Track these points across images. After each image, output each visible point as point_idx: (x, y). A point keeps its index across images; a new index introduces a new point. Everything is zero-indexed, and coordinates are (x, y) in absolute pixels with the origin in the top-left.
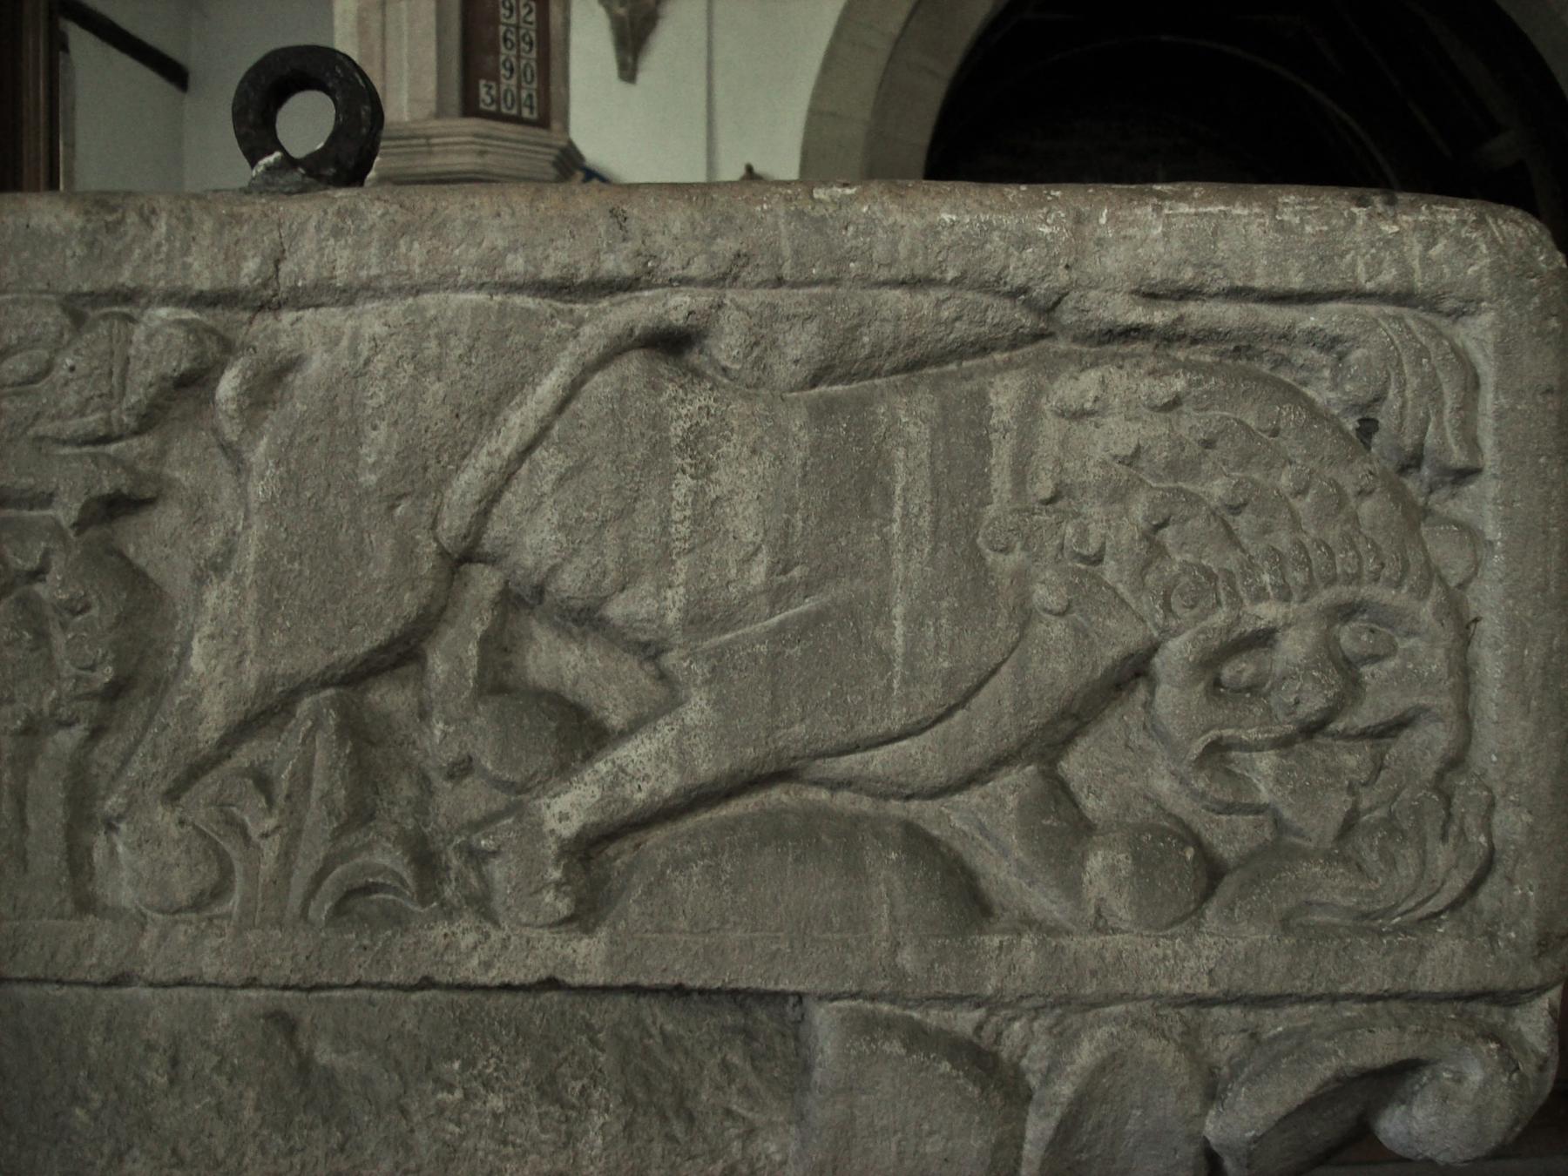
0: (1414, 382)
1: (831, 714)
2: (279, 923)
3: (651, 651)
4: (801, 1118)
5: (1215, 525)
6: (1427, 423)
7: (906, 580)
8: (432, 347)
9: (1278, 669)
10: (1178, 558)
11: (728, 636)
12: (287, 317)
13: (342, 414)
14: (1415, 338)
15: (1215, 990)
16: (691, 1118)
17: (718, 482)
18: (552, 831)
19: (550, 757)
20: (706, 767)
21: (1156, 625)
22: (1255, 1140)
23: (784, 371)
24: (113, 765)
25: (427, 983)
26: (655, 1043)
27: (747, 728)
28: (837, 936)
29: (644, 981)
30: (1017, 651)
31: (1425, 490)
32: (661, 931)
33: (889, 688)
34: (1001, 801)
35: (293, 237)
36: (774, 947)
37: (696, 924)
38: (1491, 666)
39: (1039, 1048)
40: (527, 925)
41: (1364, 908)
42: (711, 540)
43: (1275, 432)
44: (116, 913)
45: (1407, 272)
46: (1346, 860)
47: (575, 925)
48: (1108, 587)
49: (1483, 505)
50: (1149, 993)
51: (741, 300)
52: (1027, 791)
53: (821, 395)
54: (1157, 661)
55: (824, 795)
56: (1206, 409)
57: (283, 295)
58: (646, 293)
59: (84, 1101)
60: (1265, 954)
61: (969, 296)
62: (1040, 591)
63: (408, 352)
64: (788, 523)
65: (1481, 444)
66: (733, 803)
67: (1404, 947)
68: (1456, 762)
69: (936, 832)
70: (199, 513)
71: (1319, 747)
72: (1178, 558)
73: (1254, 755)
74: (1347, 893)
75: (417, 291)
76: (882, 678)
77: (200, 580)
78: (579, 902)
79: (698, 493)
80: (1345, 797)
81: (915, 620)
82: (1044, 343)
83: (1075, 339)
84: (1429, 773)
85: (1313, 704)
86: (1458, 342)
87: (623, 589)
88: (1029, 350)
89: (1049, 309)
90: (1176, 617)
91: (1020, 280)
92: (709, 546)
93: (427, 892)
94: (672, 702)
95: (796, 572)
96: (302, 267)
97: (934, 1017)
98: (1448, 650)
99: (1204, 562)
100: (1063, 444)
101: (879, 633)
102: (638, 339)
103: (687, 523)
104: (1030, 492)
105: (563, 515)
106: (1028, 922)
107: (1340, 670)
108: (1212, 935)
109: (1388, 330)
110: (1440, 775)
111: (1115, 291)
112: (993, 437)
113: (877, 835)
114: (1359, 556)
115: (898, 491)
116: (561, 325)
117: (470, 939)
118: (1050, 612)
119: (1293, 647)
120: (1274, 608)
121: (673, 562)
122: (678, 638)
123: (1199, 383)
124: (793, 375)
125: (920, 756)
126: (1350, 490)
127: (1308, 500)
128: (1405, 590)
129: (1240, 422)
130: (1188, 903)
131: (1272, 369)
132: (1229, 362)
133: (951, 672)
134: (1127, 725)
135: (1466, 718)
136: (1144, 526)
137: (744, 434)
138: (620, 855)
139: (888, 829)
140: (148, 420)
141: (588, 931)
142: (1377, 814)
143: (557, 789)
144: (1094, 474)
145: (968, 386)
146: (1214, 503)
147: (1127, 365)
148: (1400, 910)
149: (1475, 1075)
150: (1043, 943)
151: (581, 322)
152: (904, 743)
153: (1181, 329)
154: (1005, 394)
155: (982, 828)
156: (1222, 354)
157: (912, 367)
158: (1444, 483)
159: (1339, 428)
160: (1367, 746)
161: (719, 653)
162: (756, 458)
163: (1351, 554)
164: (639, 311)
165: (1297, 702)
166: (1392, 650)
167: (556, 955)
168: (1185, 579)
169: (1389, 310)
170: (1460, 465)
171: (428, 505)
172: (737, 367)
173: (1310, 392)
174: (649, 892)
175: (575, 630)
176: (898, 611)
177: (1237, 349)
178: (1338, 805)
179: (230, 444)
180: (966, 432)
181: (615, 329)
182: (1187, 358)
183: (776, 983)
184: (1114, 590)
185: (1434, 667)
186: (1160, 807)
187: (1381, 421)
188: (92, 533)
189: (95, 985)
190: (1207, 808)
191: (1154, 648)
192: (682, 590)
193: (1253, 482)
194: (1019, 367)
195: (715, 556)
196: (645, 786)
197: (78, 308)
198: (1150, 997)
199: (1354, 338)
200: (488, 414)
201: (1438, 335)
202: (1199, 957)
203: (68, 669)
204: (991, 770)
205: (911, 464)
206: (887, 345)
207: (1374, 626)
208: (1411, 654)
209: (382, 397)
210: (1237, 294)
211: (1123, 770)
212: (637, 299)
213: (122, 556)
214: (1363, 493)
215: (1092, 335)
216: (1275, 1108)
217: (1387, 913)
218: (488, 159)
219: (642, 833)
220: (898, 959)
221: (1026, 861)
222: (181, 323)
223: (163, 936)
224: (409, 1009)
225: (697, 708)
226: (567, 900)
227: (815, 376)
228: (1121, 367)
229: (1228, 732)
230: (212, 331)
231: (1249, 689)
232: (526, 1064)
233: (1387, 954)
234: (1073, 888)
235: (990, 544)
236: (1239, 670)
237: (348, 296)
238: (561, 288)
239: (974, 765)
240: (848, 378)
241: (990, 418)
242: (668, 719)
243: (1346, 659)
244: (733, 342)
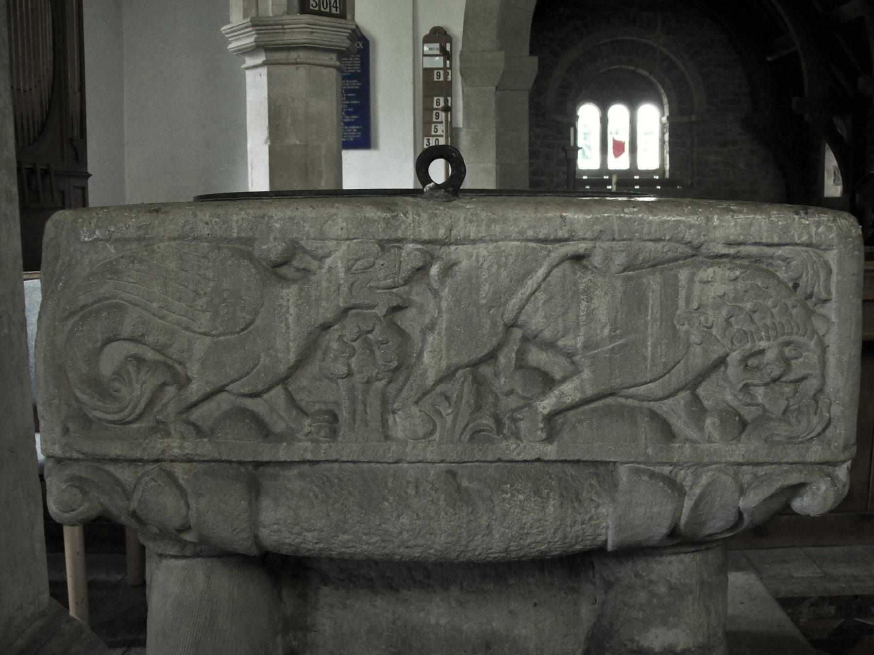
0: (811, 272)
2: (452, 442)
3: (570, 355)
4: (614, 501)
8: (503, 259)
9: (765, 361)
12: (453, 248)
13: (474, 281)
16: (580, 502)
20: (590, 392)
22: (755, 507)
23: (614, 268)
24: (394, 392)
25: (499, 460)
26: (569, 478)
29: (568, 459)
35: (455, 222)
38: (832, 361)
39: (689, 478)
43: (767, 288)
44: (397, 440)
45: (811, 237)
46: (785, 421)
49: (831, 310)
51: (602, 245)
55: (624, 400)
57: (452, 240)
59: (387, 500)
61: (673, 244)
62: (693, 337)
63: (495, 261)
68: (820, 390)
70: (422, 310)
74: (786, 431)
75: (497, 241)
77: (424, 333)
78: (548, 434)
79: (588, 307)
81: (655, 346)
83: (705, 257)
84: (811, 393)
85: (776, 373)
88: (689, 260)
89: (698, 248)
91: (689, 239)
93: (499, 431)
95: (618, 332)
96: (459, 231)
97: (657, 469)
100: (701, 291)
106: (687, 440)
110: (815, 395)
113: (641, 413)
116: (544, 253)
117: (514, 446)
119: (771, 355)
122: (580, 351)
126: (790, 306)
135: (823, 376)
138: (560, 419)
140: (406, 282)
141: (551, 443)
144: (711, 300)
145: (671, 273)
147: (722, 266)
149: (823, 488)
151: (550, 252)
154: (683, 275)
155: (672, 410)
157: (653, 266)
160: (792, 386)
161: (593, 357)
164: (570, 248)
168: (737, 334)
169: (804, 248)
171: (501, 310)
173: (778, 274)
174: (570, 431)
176: (649, 343)
178: (783, 403)
179: (435, 290)
186: (728, 404)
188: (387, 318)
189: (389, 463)
191: (727, 355)
197: (384, 245)
200: (521, 280)
201: (820, 256)
203: (381, 362)
209: (487, 276)
210: (756, 244)
211: (716, 392)
213: (396, 324)
214: (794, 307)
216: (762, 497)
217: (798, 437)
218: (315, 36)
222: (418, 250)
223: (414, 447)
224: (492, 469)
225: (586, 374)
230: (427, 252)
232: (530, 485)
234: (701, 429)
235: (678, 323)
237: (474, 242)
238: (545, 241)
239: (672, 391)
240: (634, 270)
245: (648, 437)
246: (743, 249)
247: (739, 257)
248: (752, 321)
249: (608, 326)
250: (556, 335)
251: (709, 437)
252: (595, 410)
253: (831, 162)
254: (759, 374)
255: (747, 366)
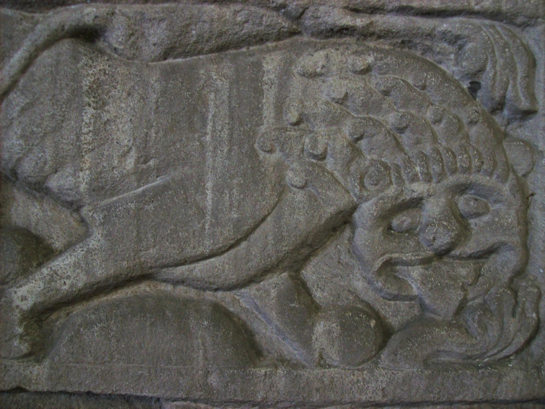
0: (501, 61)
1: (170, 243)
3: (75, 206)
5: (389, 139)
6: (508, 84)
7: (213, 168)
9: (424, 221)
10: (369, 157)
11: (115, 199)
14: (501, 37)
15: (385, 399)
17: (108, 112)
18: (18, 306)
19: (17, 265)
20: (101, 272)
21: (355, 195)
23: (149, 50)
27: (123, 251)
28: (174, 367)
29: (70, 390)
30: (276, 208)
31: (505, 122)
32: (78, 363)
33: (203, 228)
34: (267, 292)
36: (140, 372)
37: (97, 359)
40: (5, 358)
41: (469, 354)
42: (104, 144)
43: (424, 87)
46: (459, 327)
47: (32, 358)
48: (329, 173)
50: (349, 401)
51: (126, 10)
52: (282, 287)
53: (169, 64)
54: (356, 215)
55: (170, 288)
56: (385, 73)
58: (73, 7)
60: (413, 380)
61: (253, 9)
62: (290, 174)
64: (147, 134)
65: (536, 96)
66: (119, 292)
67: (490, 374)
68: (520, 273)
69: (231, 309)
71: (445, 264)
72: (369, 157)
73: (410, 268)
74: (461, 344)
76: (199, 223)
79: (97, 117)
80: (459, 292)
81: (219, 190)
82: (295, 37)
83: (313, 35)
85: (443, 240)
86: (525, 42)
87: (56, 172)
88: (287, 41)
89: (298, 18)
90: (367, 190)
92: (103, 147)
94: (87, 234)
95: (151, 163)
98: (517, 211)
99: (383, 160)
100: (304, 91)
101: (198, 198)
102: (68, 32)
103: (91, 134)
104: (284, 118)
105: (23, 130)
106: (282, 360)
107: (458, 221)
108: (384, 368)
109: (485, 33)
110: (511, 280)
111: (334, 7)
112: (265, 87)
113: (197, 311)
114: (470, 157)
115: (210, 117)
118: (295, 186)
119: (433, 208)
120: (422, 186)
121: (83, 156)
123: (381, 59)
124: (153, 52)
125: (221, 266)
126: (465, 121)
127: (442, 126)
128: (494, 177)
129: (404, 81)
130: (372, 351)
131: (422, 54)
132: (399, 49)
133: (239, 220)
134: (339, 251)
135: (526, 248)
136: (350, 138)
137: (124, 85)
138: (59, 319)
139: (204, 307)
141: (39, 361)
142: (476, 301)
143: (21, 283)
144: (321, 108)
146: (388, 127)
147: (341, 49)
148: (489, 354)
150: (289, 373)
151: (38, 22)
152: (213, 260)
153: (371, 30)
154: (272, 63)
155: (257, 308)
156: (394, 45)
157: (221, 49)
158: (516, 119)
159: (459, 86)
160: (471, 264)
161: (108, 208)
162: (130, 98)
163: (465, 156)
165: (434, 239)
166: (487, 211)
167: (21, 374)
169: (487, 22)
170: (525, 108)
172: (122, 47)
173: (443, 67)
174: (71, 341)
175: (38, 195)
176: (209, 185)
177: (403, 42)
178: (456, 296)
180: (250, 84)
181: (54, 26)
182: (375, 46)
183: (141, 392)
184: (332, 175)
185: (510, 220)
186: (357, 296)
187: (483, 83)
190: (383, 298)
191: (355, 208)
192: (88, 172)
193: (412, 116)
194: (281, 49)
195: (106, 153)
196: (68, 282)
198: (350, 403)
199: (468, 37)
201: (514, 36)
202: (377, 381)
204: (262, 275)
205: (218, 102)
206: (206, 35)
207: (477, 197)
208: (497, 213)
211: (335, 276)
212: (67, 10)
214: (472, 123)
215: (322, 32)
217: (482, 356)
219: (70, 307)
220: (209, 381)
221: (281, 327)
225: (96, 240)
226: (26, 344)
227: (165, 53)
228: (337, 50)
229: (396, 255)
231: (407, 231)
233: (481, 379)
234: (306, 342)
236: (401, 221)
239: (252, 273)
240: (185, 54)
241: (263, 76)
242: (81, 244)
243: (462, 216)
244: (119, 34)
245: (210, 355)
246: (381, 21)
247: (373, 34)
248: (398, 146)
249: (133, 154)
250: (42, 169)
251: (321, 357)
252: (117, 304)
254: (412, 243)
255: (390, 228)
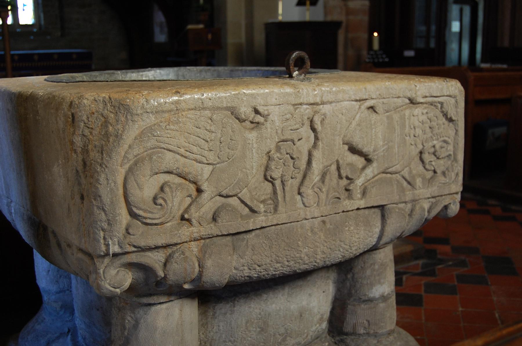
79: (375, 131)
81: (398, 147)
253: (159, 17)
